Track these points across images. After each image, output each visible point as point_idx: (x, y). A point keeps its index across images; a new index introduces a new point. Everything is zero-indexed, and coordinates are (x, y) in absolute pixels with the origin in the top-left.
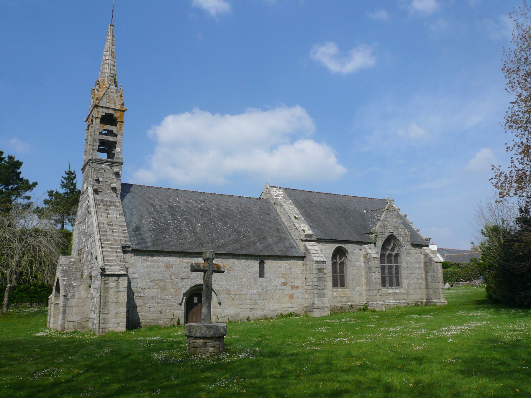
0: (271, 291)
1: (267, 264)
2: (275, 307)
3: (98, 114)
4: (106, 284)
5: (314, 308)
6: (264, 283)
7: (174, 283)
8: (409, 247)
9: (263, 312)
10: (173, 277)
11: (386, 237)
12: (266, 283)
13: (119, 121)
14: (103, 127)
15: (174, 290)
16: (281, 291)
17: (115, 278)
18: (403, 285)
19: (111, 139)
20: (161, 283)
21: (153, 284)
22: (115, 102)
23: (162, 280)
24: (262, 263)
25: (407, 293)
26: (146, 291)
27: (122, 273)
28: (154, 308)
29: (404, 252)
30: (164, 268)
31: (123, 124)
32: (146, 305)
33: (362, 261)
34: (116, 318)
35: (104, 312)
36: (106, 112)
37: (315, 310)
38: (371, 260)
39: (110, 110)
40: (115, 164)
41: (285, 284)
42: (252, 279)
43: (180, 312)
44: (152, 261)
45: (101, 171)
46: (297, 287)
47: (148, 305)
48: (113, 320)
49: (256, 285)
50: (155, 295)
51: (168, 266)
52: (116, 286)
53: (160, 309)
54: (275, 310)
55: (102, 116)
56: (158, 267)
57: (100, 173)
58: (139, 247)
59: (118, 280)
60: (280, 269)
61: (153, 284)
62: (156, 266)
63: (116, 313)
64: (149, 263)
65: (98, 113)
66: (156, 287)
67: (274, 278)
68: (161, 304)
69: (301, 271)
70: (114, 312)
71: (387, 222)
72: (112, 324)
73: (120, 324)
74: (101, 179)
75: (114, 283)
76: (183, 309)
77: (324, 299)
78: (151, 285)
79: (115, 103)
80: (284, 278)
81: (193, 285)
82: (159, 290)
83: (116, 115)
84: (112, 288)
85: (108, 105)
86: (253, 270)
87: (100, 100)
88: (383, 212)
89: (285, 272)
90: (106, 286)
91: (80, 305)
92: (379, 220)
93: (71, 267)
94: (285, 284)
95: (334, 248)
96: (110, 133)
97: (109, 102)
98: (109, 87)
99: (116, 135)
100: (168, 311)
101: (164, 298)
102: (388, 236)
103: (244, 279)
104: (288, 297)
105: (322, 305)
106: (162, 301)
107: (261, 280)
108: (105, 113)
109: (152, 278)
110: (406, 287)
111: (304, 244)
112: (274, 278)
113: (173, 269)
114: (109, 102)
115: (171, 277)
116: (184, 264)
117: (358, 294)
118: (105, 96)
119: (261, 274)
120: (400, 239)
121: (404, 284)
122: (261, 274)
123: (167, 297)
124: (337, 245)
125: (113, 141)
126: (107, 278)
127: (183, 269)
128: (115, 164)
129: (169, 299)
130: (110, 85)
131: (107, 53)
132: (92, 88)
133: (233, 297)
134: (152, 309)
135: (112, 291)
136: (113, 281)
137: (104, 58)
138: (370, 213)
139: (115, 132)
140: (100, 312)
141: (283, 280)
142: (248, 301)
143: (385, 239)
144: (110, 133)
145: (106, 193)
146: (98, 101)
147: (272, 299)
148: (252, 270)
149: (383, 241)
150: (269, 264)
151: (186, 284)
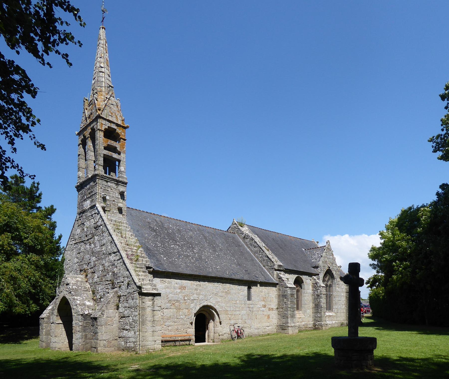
0: (255, 312)
1: (253, 289)
2: (258, 326)
3: (101, 127)
4: (143, 302)
5: (289, 327)
6: (251, 305)
7: (187, 304)
8: (339, 279)
9: (250, 330)
10: (186, 298)
11: (326, 271)
12: (252, 305)
13: (121, 138)
14: (108, 141)
15: (187, 310)
16: (262, 312)
17: (150, 298)
18: (334, 309)
19: (115, 156)
20: (177, 303)
21: (170, 304)
22: (116, 116)
23: (177, 301)
24: (249, 288)
25: (336, 316)
26: (165, 310)
27: (155, 292)
28: (172, 327)
29: (335, 283)
30: (179, 289)
31: (125, 142)
32: (165, 324)
33: (311, 289)
34: (153, 336)
35: (143, 331)
36: (109, 126)
37: (289, 328)
38: (320, 289)
39: (112, 124)
40: (120, 184)
41: (265, 306)
42: (243, 301)
43: (192, 331)
44: (169, 283)
45: (107, 189)
46: (272, 309)
47: (167, 324)
48: (151, 339)
49: (246, 306)
50: (172, 314)
51: (183, 288)
52: (153, 305)
53: (176, 327)
54: (258, 328)
55: (105, 129)
56: (175, 288)
57: (106, 191)
58: (290, 268)
59: (153, 299)
60: (261, 293)
61: (170, 304)
62: (172, 287)
63: (153, 331)
64: (166, 284)
65: (101, 126)
66: (173, 307)
67: (258, 301)
68: (176, 323)
69: (274, 295)
70: (152, 330)
71: (327, 258)
72: (150, 342)
73: (157, 341)
74: (108, 198)
75: (150, 302)
76: (194, 327)
77: (294, 319)
78: (169, 305)
79: (117, 118)
80: (264, 301)
81: (201, 305)
82: (175, 310)
83: (119, 130)
84: (148, 307)
85: (110, 118)
86: (243, 293)
87: (103, 111)
88: (324, 249)
89: (265, 296)
90: (144, 304)
91: (109, 324)
92: (322, 256)
93: (80, 287)
94: (265, 306)
95: (295, 278)
96: (114, 149)
97: (111, 114)
98: (110, 98)
99: (119, 153)
100: (182, 329)
101: (179, 318)
102: (327, 269)
103: (238, 301)
104: (266, 318)
105: (293, 324)
106: (178, 320)
107: (248, 302)
108: (108, 127)
109: (170, 299)
110: (336, 311)
111: (277, 272)
112: (258, 301)
113: (186, 290)
114: (111, 114)
115: (184, 298)
116: (194, 286)
117: (308, 316)
118: (107, 107)
119: (249, 298)
120: (334, 273)
121: (334, 309)
122: (249, 298)
123: (181, 316)
124: (298, 276)
125: (117, 158)
126: (144, 297)
127: (194, 291)
128: (120, 184)
129: (183, 318)
130: (111, 96)
131: (102, 60)
132: (34, 97)
133: (230, 317)
134: (170, 328)
135: (149, 310)
136: (149, 300)
137: (98, 65)
138: (309, 251)
139: (118, 149)
140: (139, 330)
141: (263, 303)
142: (240, 320)
143: (325, 272)
144: (114, 149)
145: (113, 213)
146: (100, 112)
147: (256, 319)
148: (243, 294)
149: (324, 273)
150: (254, 289)
151: (196, 305)
